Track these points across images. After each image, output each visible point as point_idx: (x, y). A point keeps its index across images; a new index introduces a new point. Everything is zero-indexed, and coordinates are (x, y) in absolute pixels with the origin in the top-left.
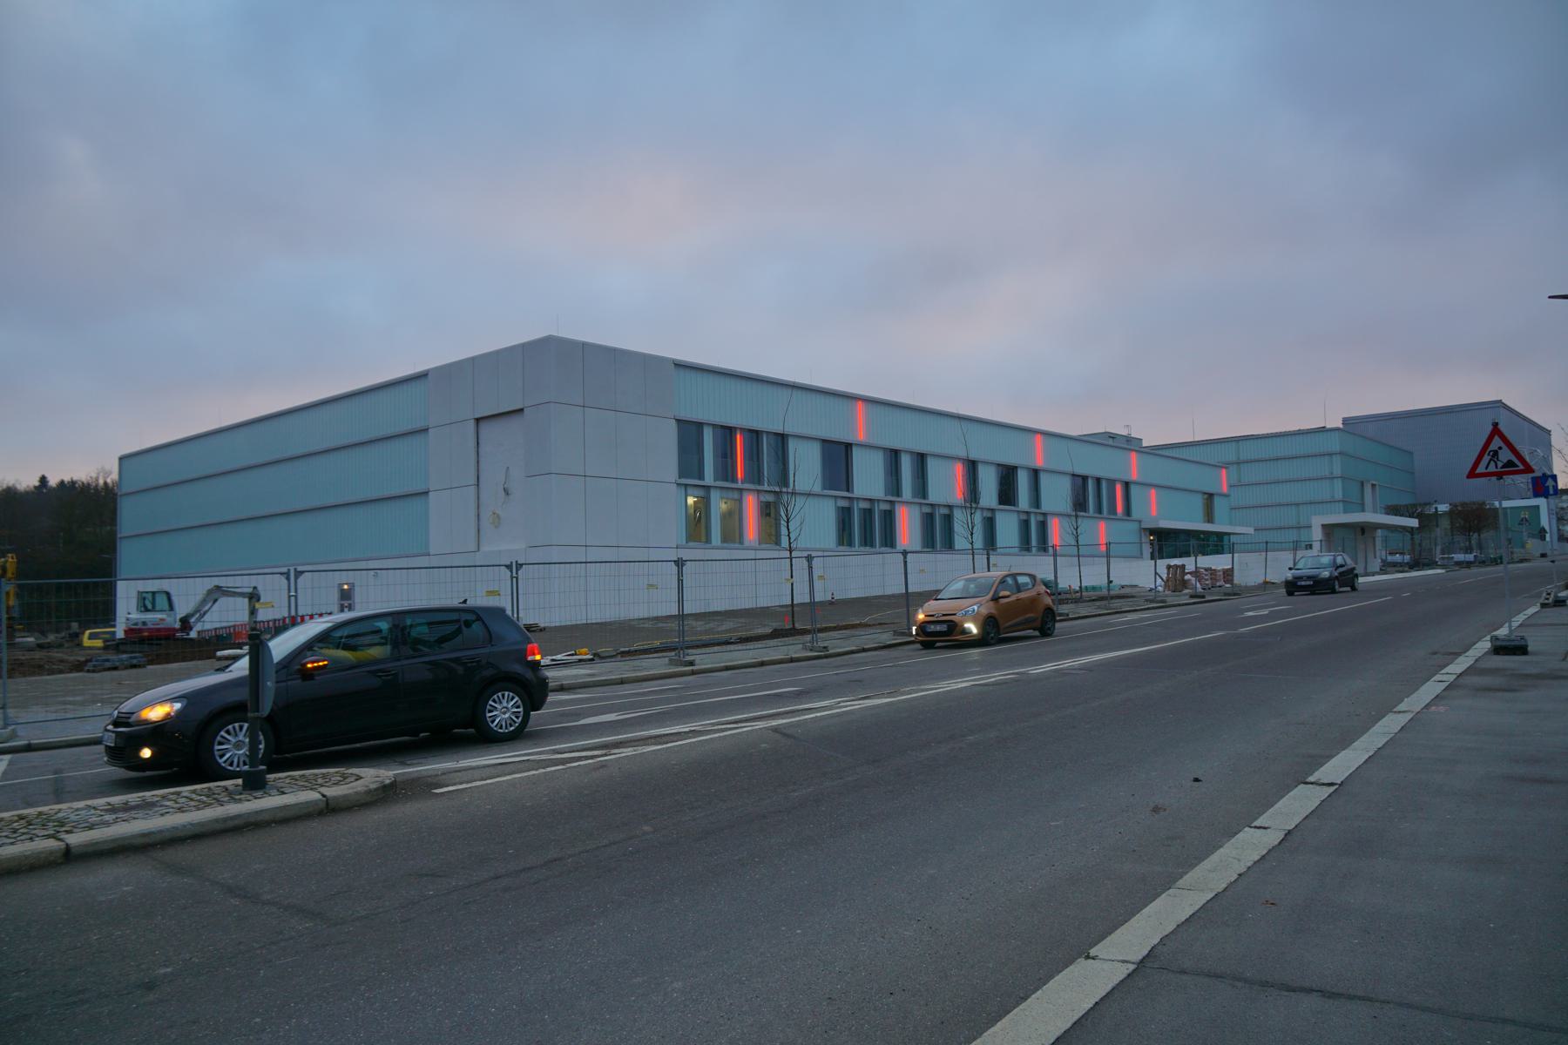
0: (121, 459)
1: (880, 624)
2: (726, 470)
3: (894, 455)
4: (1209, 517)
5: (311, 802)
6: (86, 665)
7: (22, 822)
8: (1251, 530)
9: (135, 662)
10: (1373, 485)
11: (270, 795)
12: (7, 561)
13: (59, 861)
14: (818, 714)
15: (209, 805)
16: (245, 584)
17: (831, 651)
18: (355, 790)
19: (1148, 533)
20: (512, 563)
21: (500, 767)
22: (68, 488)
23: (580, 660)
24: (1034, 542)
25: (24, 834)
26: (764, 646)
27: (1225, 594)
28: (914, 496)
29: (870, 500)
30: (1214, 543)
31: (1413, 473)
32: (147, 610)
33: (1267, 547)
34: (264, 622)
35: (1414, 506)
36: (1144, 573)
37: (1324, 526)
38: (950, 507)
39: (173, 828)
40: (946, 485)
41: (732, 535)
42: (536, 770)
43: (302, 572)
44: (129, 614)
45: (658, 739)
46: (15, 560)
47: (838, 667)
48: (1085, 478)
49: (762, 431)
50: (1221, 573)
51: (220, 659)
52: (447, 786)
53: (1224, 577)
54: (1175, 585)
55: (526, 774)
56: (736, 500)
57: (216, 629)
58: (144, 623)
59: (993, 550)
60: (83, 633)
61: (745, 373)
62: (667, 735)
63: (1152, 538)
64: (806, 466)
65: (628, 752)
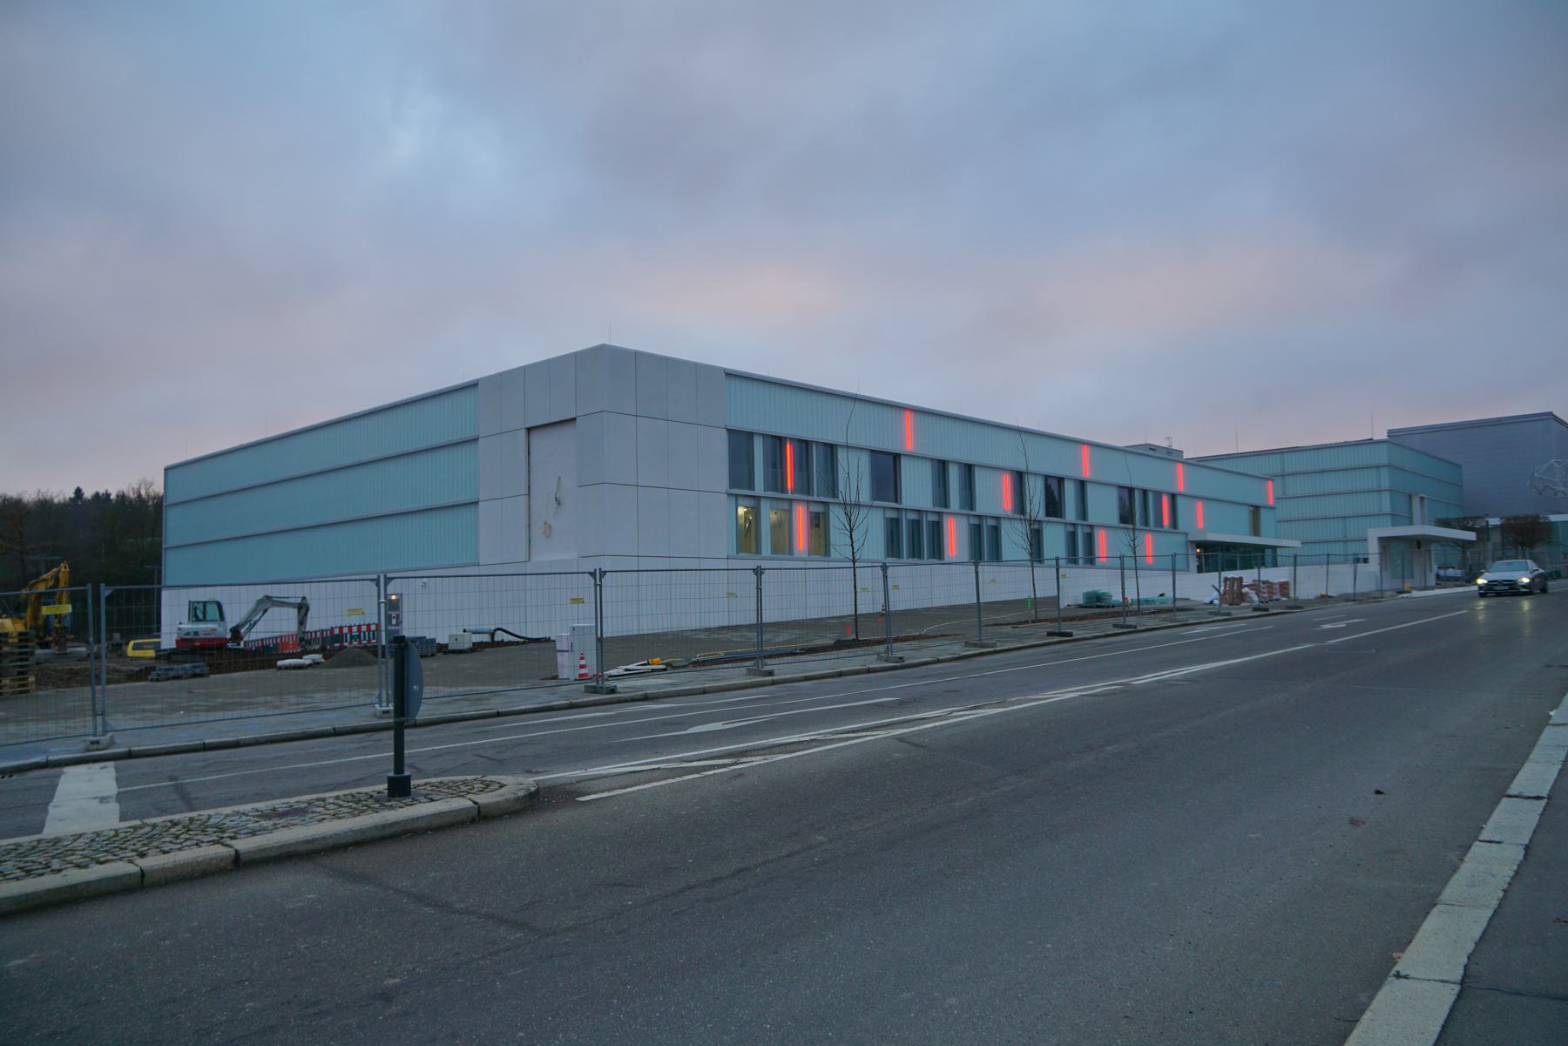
0: (167, 470)
1: (943, 635)
2: (776, 481)
3: (942, 466)
4: (1256, 531)
5: (464, 809)
6: (149, 674)
7: (180, 827)
8: (1297, 544)
9: (198, 671)
10: (1422, 498)
11: (420, 802)
12: (59, 571)
13: (229, 868)
14: (937, 724)
15: (363, 811)
16: (293, 592)
17: (907, 662)
18: (505, 797)
19: (1194, 546)
20: (595, 570)
21: (633, 775)
22: (101, 500)
23: (653, 670)
24: (1081, 553)
25: (187, 840)
26: (836, 657)
27: (1288, 607)
28: (962, 507)
29: (918, 511)
30: (1254, 556)
31: (1461, 486)
32: (198, 620)
33: (1328, 560)
34: (311, 633)
35: (1465, 519)
36: (1202, 588)
37: (1381, 539)
38: (997, 518)
39: (336, 834)
40: (994, 496)
41: (783, 546)
42: (673, 778)
43: (393, 578)
44: (180, 623)
45: (783, 747)
46: (68, 569)
47: (922, 678)
48: (1131, 490)
49: (812, 442)
50: (1277, 586)
51: (280, 668)
52: (590, 794)
53: (1281, 590)
54: (1233, 599)
55: (664, 782)
56: (785, 510)
57: (262, 640)
58: (196, 633)
59: (1040, 561)
60: (127, 644)
61: (812, 386)
62: (794, 743)
63: (1198, 551)
64: (855, 475)
65: (757, 760)
